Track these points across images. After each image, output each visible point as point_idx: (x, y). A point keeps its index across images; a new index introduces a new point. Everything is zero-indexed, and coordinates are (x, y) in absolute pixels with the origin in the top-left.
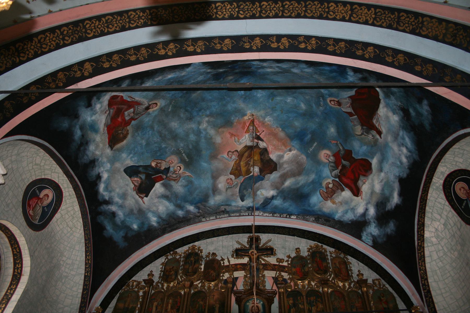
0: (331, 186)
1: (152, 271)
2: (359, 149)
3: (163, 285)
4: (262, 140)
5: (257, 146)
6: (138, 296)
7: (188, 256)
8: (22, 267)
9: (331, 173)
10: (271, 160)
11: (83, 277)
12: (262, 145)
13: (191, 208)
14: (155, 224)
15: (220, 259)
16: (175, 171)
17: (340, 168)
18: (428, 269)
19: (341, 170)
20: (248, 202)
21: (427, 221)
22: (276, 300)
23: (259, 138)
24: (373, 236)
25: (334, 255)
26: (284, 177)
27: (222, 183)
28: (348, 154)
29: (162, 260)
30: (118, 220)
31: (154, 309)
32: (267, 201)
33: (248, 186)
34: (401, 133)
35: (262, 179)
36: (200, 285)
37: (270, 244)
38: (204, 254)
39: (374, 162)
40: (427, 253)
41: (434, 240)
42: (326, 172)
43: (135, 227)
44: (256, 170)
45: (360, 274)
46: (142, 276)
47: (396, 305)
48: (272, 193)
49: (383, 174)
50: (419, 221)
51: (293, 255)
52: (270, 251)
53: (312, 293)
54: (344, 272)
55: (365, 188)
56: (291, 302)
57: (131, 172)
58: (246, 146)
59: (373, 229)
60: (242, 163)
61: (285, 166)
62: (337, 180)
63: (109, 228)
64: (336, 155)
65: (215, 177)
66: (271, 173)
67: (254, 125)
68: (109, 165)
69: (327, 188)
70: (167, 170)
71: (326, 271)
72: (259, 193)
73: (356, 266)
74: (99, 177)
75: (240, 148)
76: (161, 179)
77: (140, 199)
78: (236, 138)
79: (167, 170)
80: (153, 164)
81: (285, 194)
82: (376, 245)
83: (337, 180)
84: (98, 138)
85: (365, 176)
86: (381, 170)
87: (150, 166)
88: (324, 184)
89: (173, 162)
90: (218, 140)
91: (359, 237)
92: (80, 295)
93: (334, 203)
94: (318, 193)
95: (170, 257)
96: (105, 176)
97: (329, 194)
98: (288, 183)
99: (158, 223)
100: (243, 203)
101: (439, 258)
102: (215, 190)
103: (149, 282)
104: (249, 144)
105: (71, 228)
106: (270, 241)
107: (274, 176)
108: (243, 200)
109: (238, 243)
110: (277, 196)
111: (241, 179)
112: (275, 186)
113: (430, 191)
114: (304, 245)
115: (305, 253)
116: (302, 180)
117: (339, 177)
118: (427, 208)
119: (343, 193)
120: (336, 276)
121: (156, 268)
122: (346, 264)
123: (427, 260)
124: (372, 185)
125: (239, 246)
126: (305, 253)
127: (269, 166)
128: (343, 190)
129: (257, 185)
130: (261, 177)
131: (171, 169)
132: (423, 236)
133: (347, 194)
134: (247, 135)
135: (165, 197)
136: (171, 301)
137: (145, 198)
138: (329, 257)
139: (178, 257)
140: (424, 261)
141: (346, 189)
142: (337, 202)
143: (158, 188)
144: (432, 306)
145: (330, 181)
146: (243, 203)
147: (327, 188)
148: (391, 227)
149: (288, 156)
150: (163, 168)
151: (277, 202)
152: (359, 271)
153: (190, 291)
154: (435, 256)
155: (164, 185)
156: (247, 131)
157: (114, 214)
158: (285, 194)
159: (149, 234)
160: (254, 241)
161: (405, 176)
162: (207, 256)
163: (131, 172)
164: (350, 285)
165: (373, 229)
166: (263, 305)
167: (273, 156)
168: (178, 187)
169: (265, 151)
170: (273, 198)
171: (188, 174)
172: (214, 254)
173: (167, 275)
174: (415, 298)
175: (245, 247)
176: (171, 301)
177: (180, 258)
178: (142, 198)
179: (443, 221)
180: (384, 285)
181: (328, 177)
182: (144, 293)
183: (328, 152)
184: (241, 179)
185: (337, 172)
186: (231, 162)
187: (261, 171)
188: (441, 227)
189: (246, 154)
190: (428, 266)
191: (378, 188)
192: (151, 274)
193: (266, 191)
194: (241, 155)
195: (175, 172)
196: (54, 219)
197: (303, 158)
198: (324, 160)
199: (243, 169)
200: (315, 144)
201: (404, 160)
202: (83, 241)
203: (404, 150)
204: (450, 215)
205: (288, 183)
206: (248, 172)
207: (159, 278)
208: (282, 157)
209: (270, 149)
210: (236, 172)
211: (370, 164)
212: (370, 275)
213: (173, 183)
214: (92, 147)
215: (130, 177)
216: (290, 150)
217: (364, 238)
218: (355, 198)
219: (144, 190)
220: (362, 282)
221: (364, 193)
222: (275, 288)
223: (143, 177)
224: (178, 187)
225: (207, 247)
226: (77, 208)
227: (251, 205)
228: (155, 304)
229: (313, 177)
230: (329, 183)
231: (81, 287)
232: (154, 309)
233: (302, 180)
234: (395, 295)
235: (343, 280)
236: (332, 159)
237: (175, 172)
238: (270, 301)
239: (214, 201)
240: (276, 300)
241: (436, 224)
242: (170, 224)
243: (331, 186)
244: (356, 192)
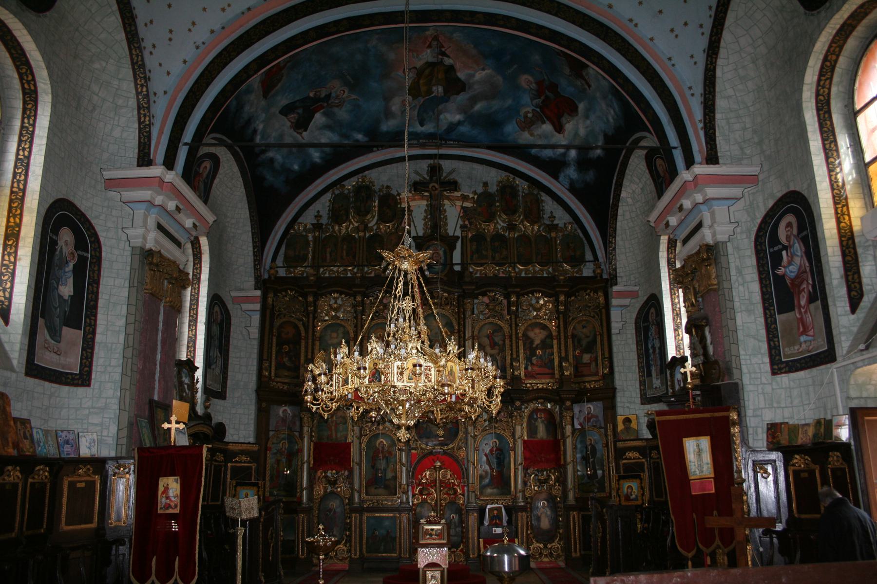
0: (530, 115)
1: (318, 212)
2: (567, 87)
3: (333, 227)
4: (448, 57)
5: (442, 62)
6: (307, 243)
7: (358, 189)
8: (200, 246)
9: (532, 100)
10: (459, 80)
11: (250, 234)
12: (448, 61)
13: (360, 137)
14: (318, 160)
15: (395, 193)
16: (338, 96)
17: (543, 98)
18: (618, 227)
19: (544, 101)
20: (429, 128)
21: (626, 182)
22: (459, 245)
23: (444, 54)
24: (571, 179)
25: (526, 192)
26: (474, 100)
27: (395, 106)
28: (553, 87)
29: (328, 196)
30: (277, 166)
31: (328, 255)
32: (452, 127)
33: (428, 108)
34: (610, 97)
35: (447, 101)
36: (375, 228)
37: (451, 177)
38: (376, 188)
39: (581, 106)
40: (620, 212)
41: (630, 201)
42: (526, 99)
43: (296, 167)
44: (438, 90)
45: (552, 217)
46: (308, 218)
47: (583, 255)
48: (458, 117)
49: (588, 122)
50: (617, 181)
51: (480, 190)
52: (454, 185)
53: (498, 237)
54: (534, 213)
55: (569, 127)
56: (474, 247)
57: (286, 111)
58: (427, 63)
59: (572, 172)
60: (421, 82)
61: (476, 87)
62: (538, 110)
63: (269, 177)
64: (539, 83)
65: (387, 99)
66: (458, 93)
67: (438, 40)
68: (264, 115)
69: (526, 117)
70: (328, 96)
71: (514, 212)
72: (442, 117)
73: (549, 205)
74: (255, 131)
75: (419, 64)
76: (322, 107)
77: (298, 136)
78: (415, 54)
79: (328, 96)
80: (312, 95)
81: (474, 120)
82: (573, 189)
83: (538, 110)
84: (252, 97)
85: (570, 115)
86: (587, 117)
87: (308, 98)
88: (522, 113)
89: (337, 88)
90: (392, 56)
91: (556, 178)
92: (251, 253)
93: (532, 135)
94: (514, 122)
95: (337, 192)
96: (261, 127)
97: (528, 124)
98: (478, 107)
99: (321, 158)
100: (423, 129)
101: (631, 218)
102: (388, 114)
103: (317, 226)
104: (431, 60)
105: (231, 189)
106: (453, 171)
107: (462, 98)
108: (422, 125)
109: (417, 173)
110: (464, 121)
111: (421, 100)
112: (462, 110)
113: (632, 157)
114: (494, 176)
115: (493, 189)
116: (496, 105)
117: (541, 108)
118: (627, 171)
119: (544, 126)
120: (526, 218)
121: (323, 206)
122: (538, 202)
123: (619, 218)
124: (577, 128)
125: (418, 178)
126: (493, 189)
127: (455, 86)
128: (544, 122)
129: (440, 107)
130: (445, 99)
131: (333, 95)
132: (619, 195)
133: (547, 127)
134: (429, 51)
135: (328, 127)
136: (345, 247)
137: (304, 133)
138: (520, 194)
139: (346, 192)
140: (616, 219)
141: (547, 122)
142: (535, 134)
143: (319, 118)
144: (710, 122)
145: (529, 109)
146: (423, 129)
147: (526, 117)
148: (590, 176)
149: (479, 75)
150: (323, 96)
151: (464, 129)
152: (552, 212)
153: (365, 234)
154: (628, 216)
155: (326, 114)
156: (430, 46)
157: (272, 160)
158: (474, 120)
159: (314, 172)
160: (434, 170)
161: (610, 134)
162: (380, 190)
163: (286, 111)
164: (539, 227)
165: (572, 172)
166: (445, 252)
167: (461, 75)
168: (343, 114)
169: (451, 69)
170: (459, 123)
171: (354, 97)
172: (388, 187)
173: (337, 215)
174: (601, 254)
175: (424, 178)
176: (345, 247)
177: (349, 192)
178: (301, 134)
179: (641, 185)
180: (576, 230)
181: (528, 106)
182: (314, 237)
183: (530, 78)
184: (421, 100)
185: (538, 101)
186: (408, 79)
187: (446, 91)
188: (638, 191)
189: (427, 72)
190: (619, 224)
191: (582, 132)
192: (318, 216)
193: (451, 116)
194: (420, 73)
195: (337, 97)
196: (214, 185)
197: (499, 79)
198: (524, 85)
199: (423, 89)
200: (515, 66)
201: (611, 120)
202: (245, 198)
203: (612, 112)
204: (648, 182)
205: (478, 107)
206: (429, 92)
207: (329, 218)
208: (474, 76)
209: (458, 66)
210: (414, 91)
211: (577, 107)
212: (561, 218)
213: (336, 110)
214: (247, 108)
215: (286, 116)
216: (483, 69)
217: (561, 179)
218: (557, 134)
219: (302, 125)
220: (553, 227)
221: (567, 132)
222: (458, 233)
223: (300, 111)
224: (343, 114)
225: (380, 178)
226: (236, 169)
227: (432, 130)
228: (328, 250)
229: (509, 102)
230: (529, 112)
231: (251, 244)
232: (328, 255)
233: (496, 105)
234: (585, 242)
235: (533, 223)
236: (534, 86)
237: (337, 97)
238: (452, 248)
239: (387, 126)
240: (459, 245)
241: (634, 187)
242: (338, 155)
243: (530, 115)
244: (559, 129)
